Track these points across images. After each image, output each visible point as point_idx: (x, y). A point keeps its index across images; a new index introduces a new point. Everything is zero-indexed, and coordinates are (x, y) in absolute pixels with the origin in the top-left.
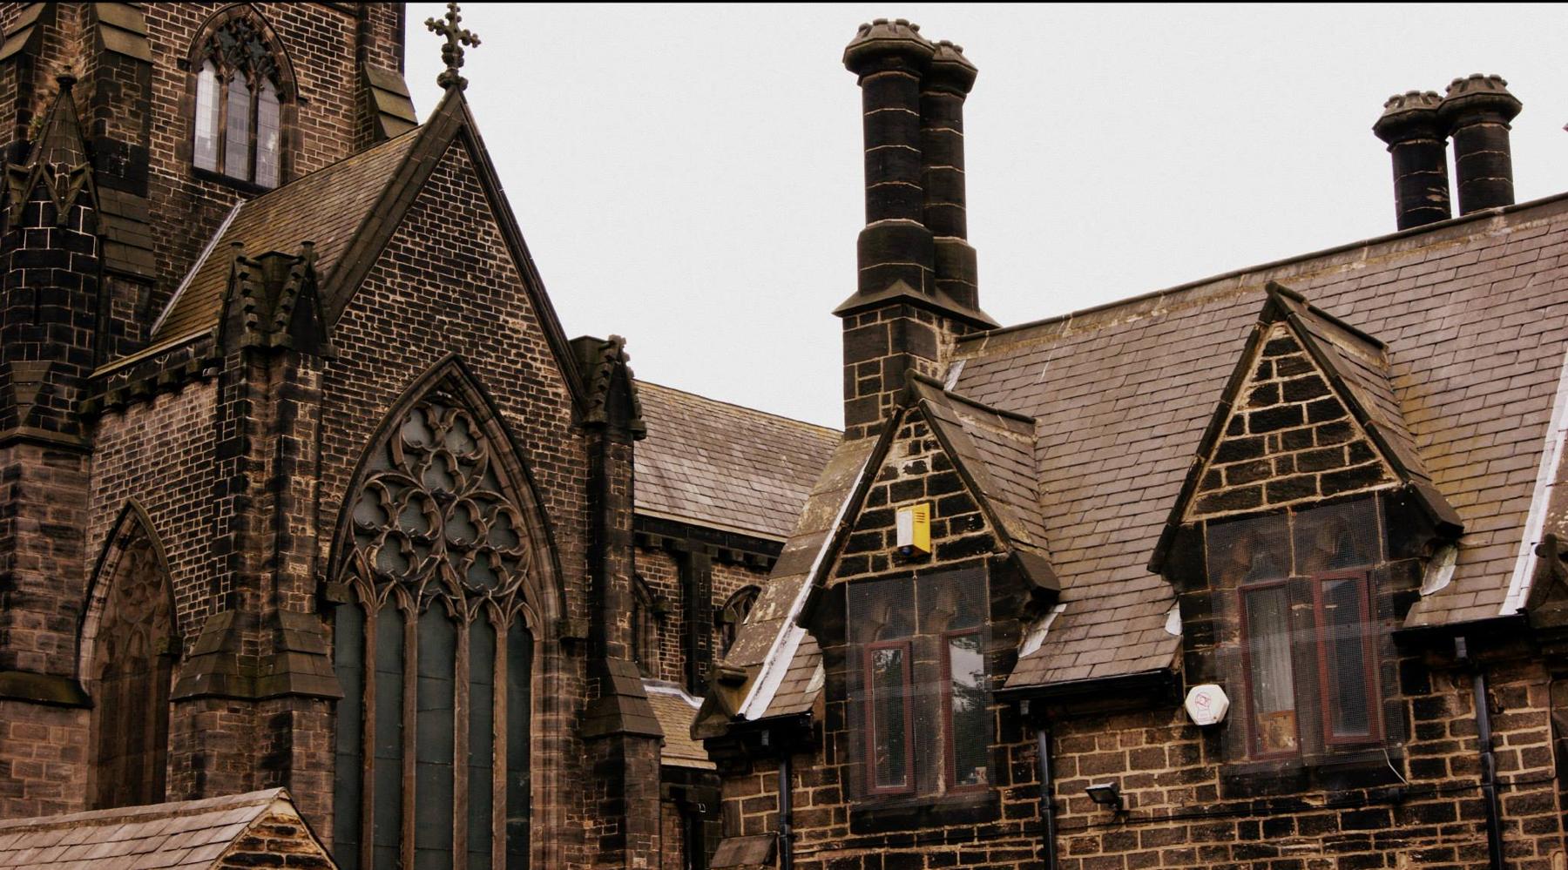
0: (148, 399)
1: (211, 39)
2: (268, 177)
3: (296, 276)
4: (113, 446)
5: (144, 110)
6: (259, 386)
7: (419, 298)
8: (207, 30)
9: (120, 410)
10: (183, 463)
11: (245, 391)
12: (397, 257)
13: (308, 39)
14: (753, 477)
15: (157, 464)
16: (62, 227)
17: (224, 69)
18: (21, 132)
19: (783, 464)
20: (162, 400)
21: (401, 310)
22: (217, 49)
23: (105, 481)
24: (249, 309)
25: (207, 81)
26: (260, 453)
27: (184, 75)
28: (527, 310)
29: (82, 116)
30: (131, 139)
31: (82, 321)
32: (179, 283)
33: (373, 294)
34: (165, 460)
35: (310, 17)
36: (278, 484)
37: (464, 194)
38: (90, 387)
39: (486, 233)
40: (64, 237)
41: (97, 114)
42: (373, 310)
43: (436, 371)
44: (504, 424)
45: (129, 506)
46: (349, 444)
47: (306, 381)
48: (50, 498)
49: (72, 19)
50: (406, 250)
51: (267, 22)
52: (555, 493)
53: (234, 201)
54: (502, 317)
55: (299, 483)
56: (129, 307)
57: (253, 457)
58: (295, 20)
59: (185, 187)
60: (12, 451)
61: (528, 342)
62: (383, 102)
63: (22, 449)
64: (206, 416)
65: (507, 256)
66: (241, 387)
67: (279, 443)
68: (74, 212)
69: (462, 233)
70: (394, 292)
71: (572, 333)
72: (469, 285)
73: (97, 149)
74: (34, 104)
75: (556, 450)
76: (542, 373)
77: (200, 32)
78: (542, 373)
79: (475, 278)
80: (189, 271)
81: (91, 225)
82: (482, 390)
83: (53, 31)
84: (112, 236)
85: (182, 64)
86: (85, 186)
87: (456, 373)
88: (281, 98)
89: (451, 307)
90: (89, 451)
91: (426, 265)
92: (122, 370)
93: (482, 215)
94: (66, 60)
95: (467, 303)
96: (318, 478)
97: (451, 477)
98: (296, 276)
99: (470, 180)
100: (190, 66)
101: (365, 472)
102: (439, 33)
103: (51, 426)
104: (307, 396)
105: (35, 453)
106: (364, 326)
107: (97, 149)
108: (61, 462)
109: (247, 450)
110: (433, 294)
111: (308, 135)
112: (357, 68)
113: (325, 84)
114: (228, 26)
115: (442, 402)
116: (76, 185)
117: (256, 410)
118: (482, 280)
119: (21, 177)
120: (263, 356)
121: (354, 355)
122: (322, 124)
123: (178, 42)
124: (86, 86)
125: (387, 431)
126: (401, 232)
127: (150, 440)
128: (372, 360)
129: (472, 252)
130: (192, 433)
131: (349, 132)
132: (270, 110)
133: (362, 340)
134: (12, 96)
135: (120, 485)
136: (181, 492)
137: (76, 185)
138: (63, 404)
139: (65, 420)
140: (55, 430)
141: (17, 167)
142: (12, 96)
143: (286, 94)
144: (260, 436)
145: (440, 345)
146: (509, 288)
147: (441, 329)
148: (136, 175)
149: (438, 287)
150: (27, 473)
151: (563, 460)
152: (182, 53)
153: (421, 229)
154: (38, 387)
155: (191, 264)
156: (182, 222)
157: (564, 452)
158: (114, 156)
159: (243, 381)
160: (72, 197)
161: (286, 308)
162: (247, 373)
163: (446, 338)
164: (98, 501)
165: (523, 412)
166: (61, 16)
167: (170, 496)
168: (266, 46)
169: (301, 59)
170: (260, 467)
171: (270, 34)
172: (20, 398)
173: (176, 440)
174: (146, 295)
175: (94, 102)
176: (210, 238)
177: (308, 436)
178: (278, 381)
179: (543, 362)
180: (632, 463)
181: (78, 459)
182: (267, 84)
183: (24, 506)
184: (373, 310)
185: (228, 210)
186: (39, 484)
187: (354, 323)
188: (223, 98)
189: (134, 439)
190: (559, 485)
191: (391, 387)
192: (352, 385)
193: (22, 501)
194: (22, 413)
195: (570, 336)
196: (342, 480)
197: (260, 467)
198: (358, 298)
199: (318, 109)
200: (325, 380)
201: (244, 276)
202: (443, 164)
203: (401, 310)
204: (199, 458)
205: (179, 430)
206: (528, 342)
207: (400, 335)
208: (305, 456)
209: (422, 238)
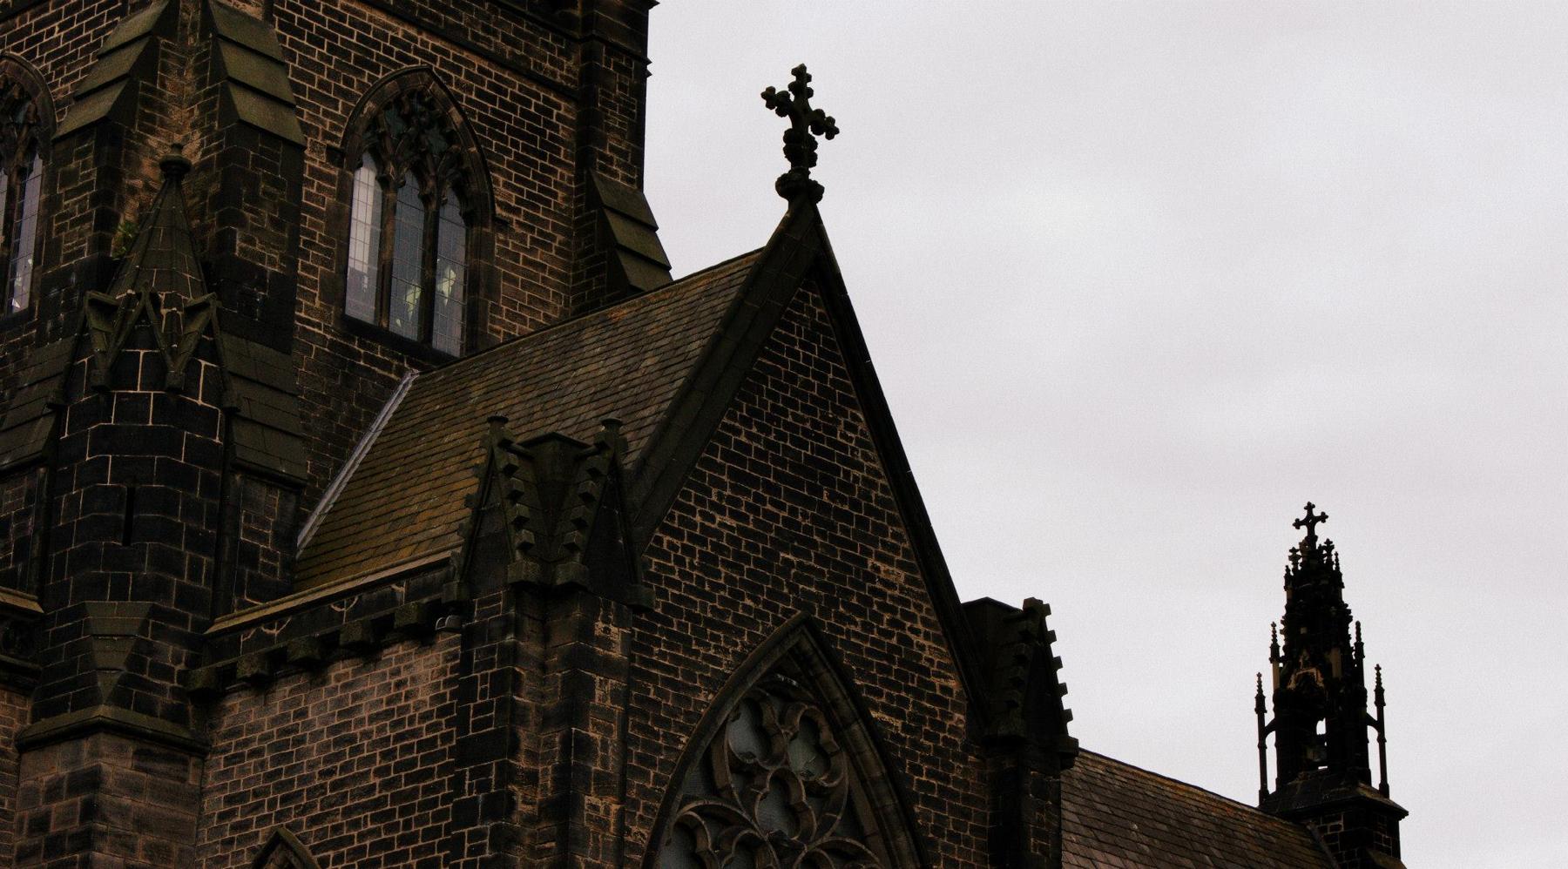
0: (315, 670)
1: (374, 122)
2: (448, 338)
3: (594, 473)
4: (246, 743)
5: (291, 214)
6: (532, 648)
7: (756, 522)
8: (370, 105)
9: (261, 686)
10: (378, 773)
11: (512, 654)
12: (727, 456)
13: (511, 131)
14: (1097, 854)
15: (331, 772)
16: (174, 390)
17: (391, 168)
18: (101, 244)
19: (1134, 836)
20: (341, 670)
21: (731, 539)
22: (382, 136)
23: (229, 800)
24: (520, 523)
25: (365, 184)
26: (532, 756)
27: (335, 172)
28: (906, 553)
29: (196, 222)
30: (272, 263)
31: (197, 543)
32: (321, 496)
33: (692, 511)
34: (344, 769)
35: (513, 95)
36: (563, 808)
37: (818, 364)
38: (202, 646)
39: (849, 427)
40: (174, 407)
41: (222, 222)
42: (692, 537)
43: (779, 641)
44: (872, 727)
45: (276, 841)
46: (658, 750)
47: (607, 643)
48: (142, 824)
49: (180, 74)
50: (739, 444)
51: (454, 99)
52: (946, 848)
53: (401, 372)
54: (870, 561)
55: (595, 808)
56: (265, 524)
57: (522, 763)
58: (492, 100)
59: (333, 344)
60: (86, 745)
61: (906, 603)
62: (622, 231)
63: (104, 741)
64: (424, 695)
65: (877, 466)
66: (503, 648)
67: (566, 742)
68: (192, 367)
69: (815, 424)
70: (722, 511)
71: (967, 592)
72: (824, 507)
73: (220, 271)
74: (122, 203)
75: (946, 779)
76: (926, 654)
77: (360, 108)
78: (926, 654)
79: (833, 496)
80: (335, 475)
81: (216, 391)
82: (844, 677)
83: (153, 91)
84: (244, 413)
85: (334, 156)
86: (209, 329)
87: (806, 646)
88: (469, 219)
89: (802, 540)
90: (199, 750)
91: (765, 471)
92: (269, 621)
93: (843, 399)
94: (169, 137)
95: (822, 534)
96: (622, 800)
97: (793, 813)
98: (594, 473)
99: (826, 342)
100: (345, 159)
101: (679, 798)
102: (781, 113)
103: (147, 708)
104: (608, 667)
105: (121, 749)
106: (679, 561)
107: (220, 271)
108: (161, 767)
109: (514, 749)
110: (775, 517)
111: (507, 278)
112: (578, 179)
113: (532, 201)
114: (398, 102)
115: (786, 697)
116: (196, 326)
117: (527, 685)
118: (843, 500)
119: (106, 310)
120: (542, 598)
121: (666, 607)
122: (526, 261)
123: (329, 121)
124: (203, 176)
125: (711, 730)
126: (732, 417)
127: (316, 736)
128: (692, 617)
129: (830, 455)
130: (400, 723)
131: (564, 277)
132: (453, 236)
133: (676, 584)
134: (88, 186)
135: (259, 806)
136: (374, 819)
137: (196, 326)
138: (166, 673)
139: (168, 699)
140: (151, 713)
141: (99, 296)
142: (88, 186)
143: (477, 213)
144: (532, 729)
145: (785, 599)
146: (879, 515)
147: (787, 575)
148: (277, 326)
149: (781, 507)
150: (110, 782)
151: (954, 795)
152: (334, 138)
153: (758, 414)
154: (128, 646)
155: (339, 467)
156: (325, 400)
157: (956, 782)
158: (246, 286)
159: (510, 638)
160: (190, 345)
161: (580, 524)
162: (514, 626)
163: (793, 589)
164: (218, 831)
165: (899, 714)
166: (165, 69)
167: (355, 824)
168: (450, 138)
169: (501, 161)
170: (532, 778)
171: (457, 118)
172: (101, 660)
173: (366, 735)
174: (291, 507)
175: (218, 201)
176: (367, 428)
177: (608, 731)
178: (564, 640)
179: (927, 636)
180: (1058, 804)
181: (185, 763)
182: (450, 195)
183: (103, 834)
184: (692, 537)
185: (392, 385)
186: (126, 801)
187: (666, 556)
188: (387, 213)
189: (287, 732)
190: (952, 836)
191: (717, 662)
192: (662, 655)
193: (102, 827)
194: (105, 684)
195: (966, 595)
196: (646, 808)
197: (532, 778)
198: (672, 517)
199: (522, 238)
200: (630, 644)
201: (510, 470)
202: (789, 315)
203: (731, 539)
204: (413, 763)
205: (372, 719)
206: (906, 603)
207: (729, 579)
208: (605, 765)
209: (761, 428)
